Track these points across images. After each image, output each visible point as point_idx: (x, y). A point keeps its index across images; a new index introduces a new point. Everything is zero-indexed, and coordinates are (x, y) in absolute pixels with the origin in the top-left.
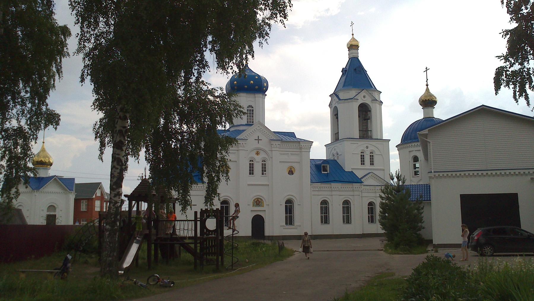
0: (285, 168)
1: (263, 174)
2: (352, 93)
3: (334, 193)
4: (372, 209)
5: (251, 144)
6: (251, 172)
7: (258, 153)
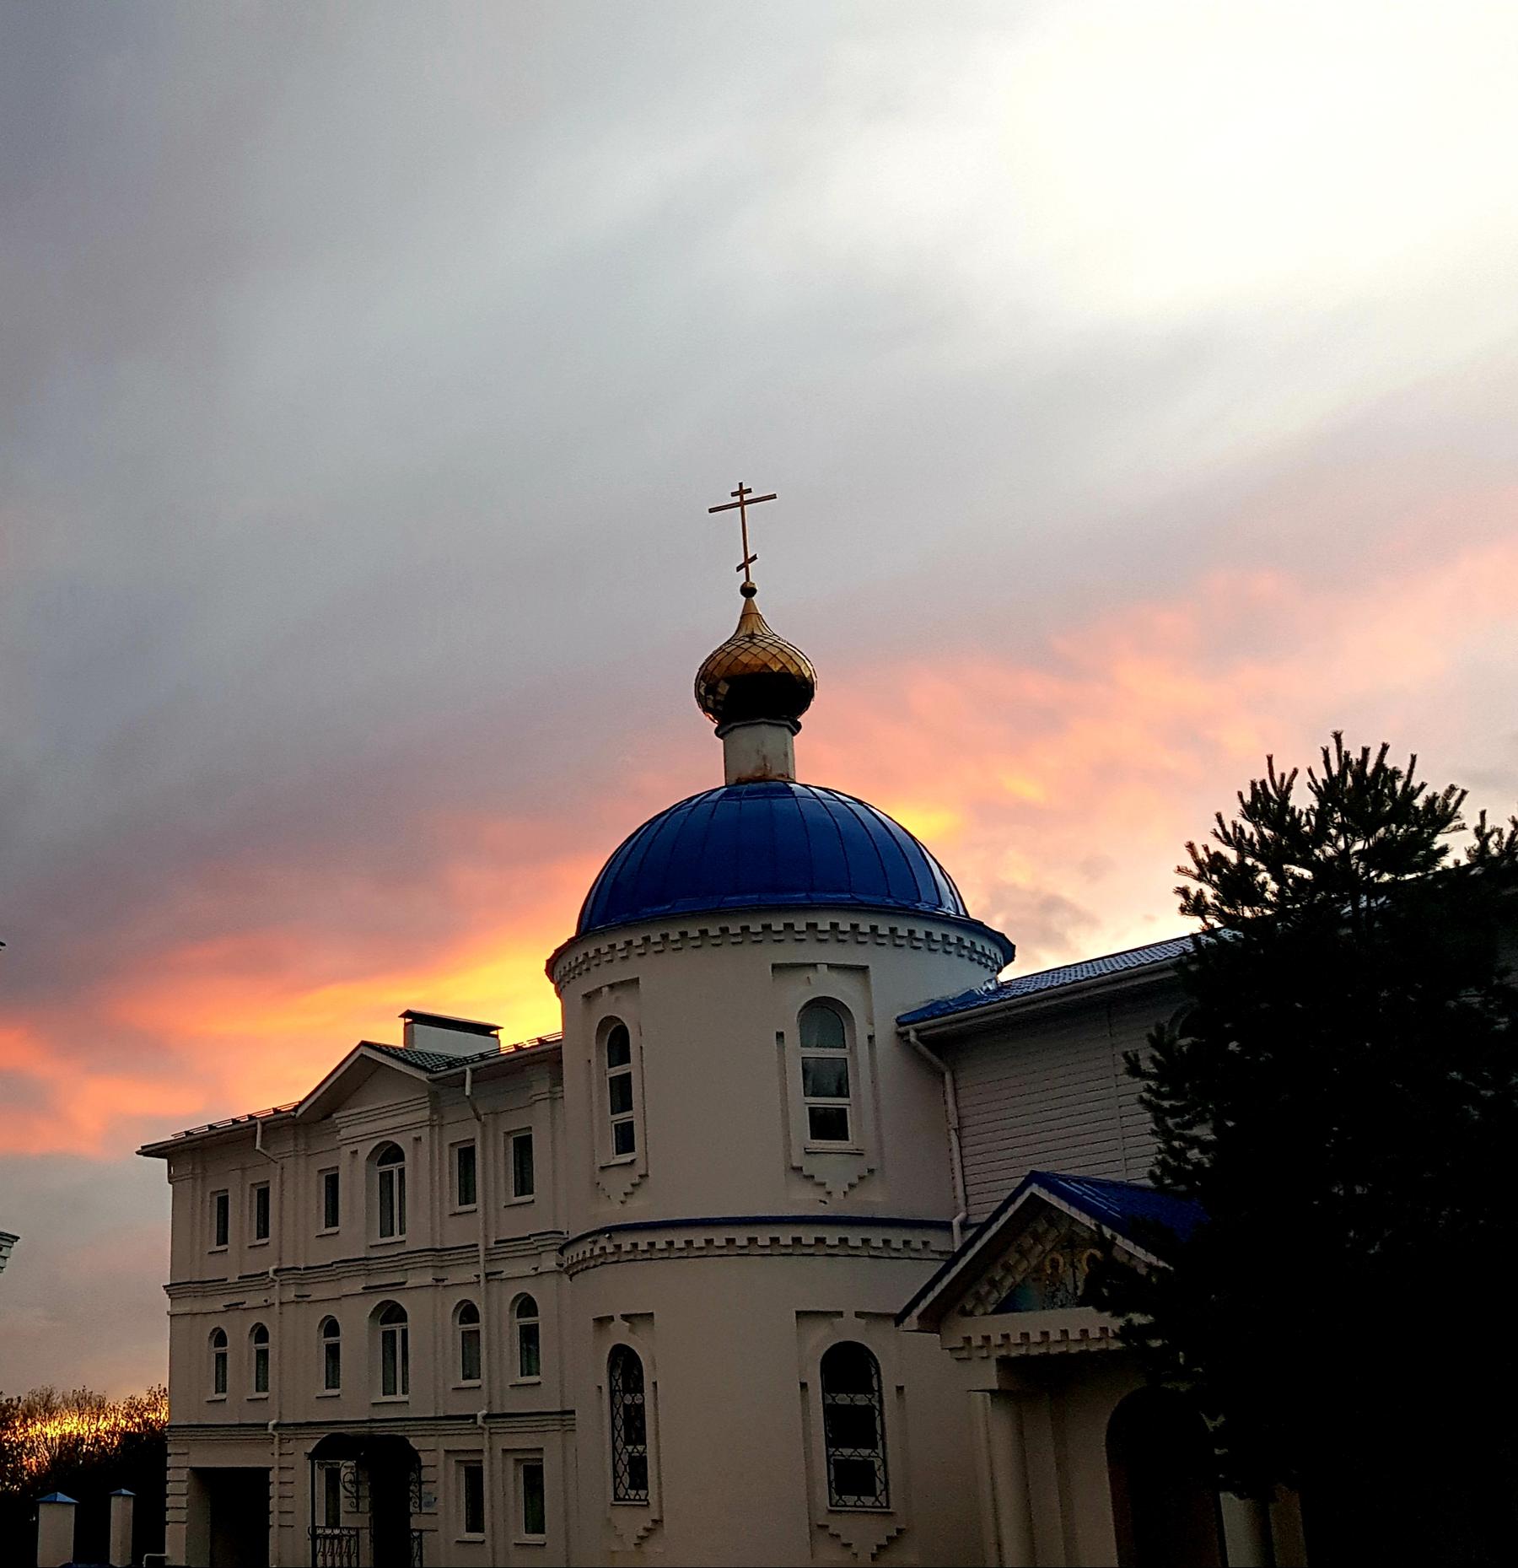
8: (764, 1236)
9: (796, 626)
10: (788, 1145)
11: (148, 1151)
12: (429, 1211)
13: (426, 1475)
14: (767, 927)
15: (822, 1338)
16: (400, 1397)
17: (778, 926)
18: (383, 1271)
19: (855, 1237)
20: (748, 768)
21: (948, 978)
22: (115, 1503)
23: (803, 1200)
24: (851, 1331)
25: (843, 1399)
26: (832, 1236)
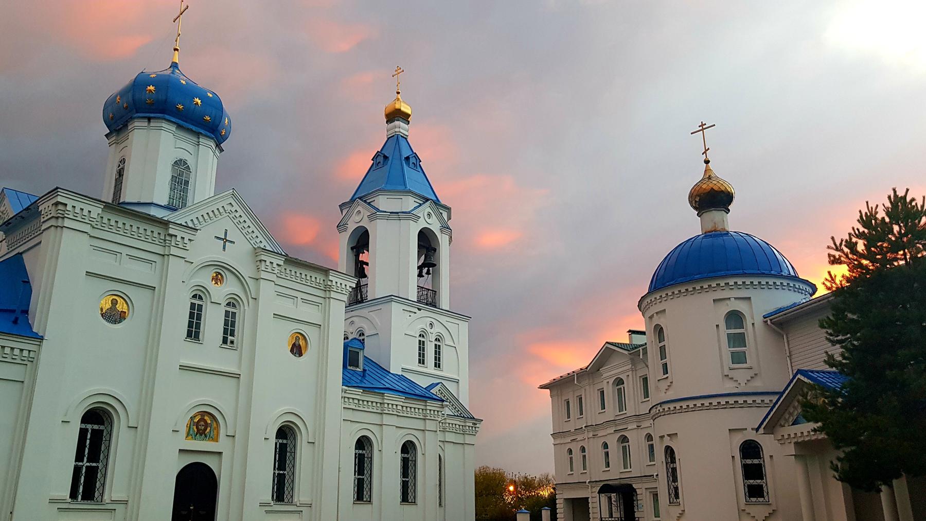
0: (284, 335)
1: (225, 341)
2: (409, 203)
3: (387, 419)
4: (98, 438)
5: (204, 247)
6: (194, 332)
7: (218, 278)
8: (715, 401)
9: (726, 174)
10: (722, 367)
11: (542, 387)
12: (635, 404)
13: (639, 497)
14: (710, 286)
15: (739, 439)
16: (629, 470)
17: (714, 285)
18: (620, 424)
19: (750, 400)
20: (709, 227)
21: (787, 298)
22: (544, 512)
23: (729, 387)
24: (751, 435)
25: (749, 461)
26: (741, 400)
